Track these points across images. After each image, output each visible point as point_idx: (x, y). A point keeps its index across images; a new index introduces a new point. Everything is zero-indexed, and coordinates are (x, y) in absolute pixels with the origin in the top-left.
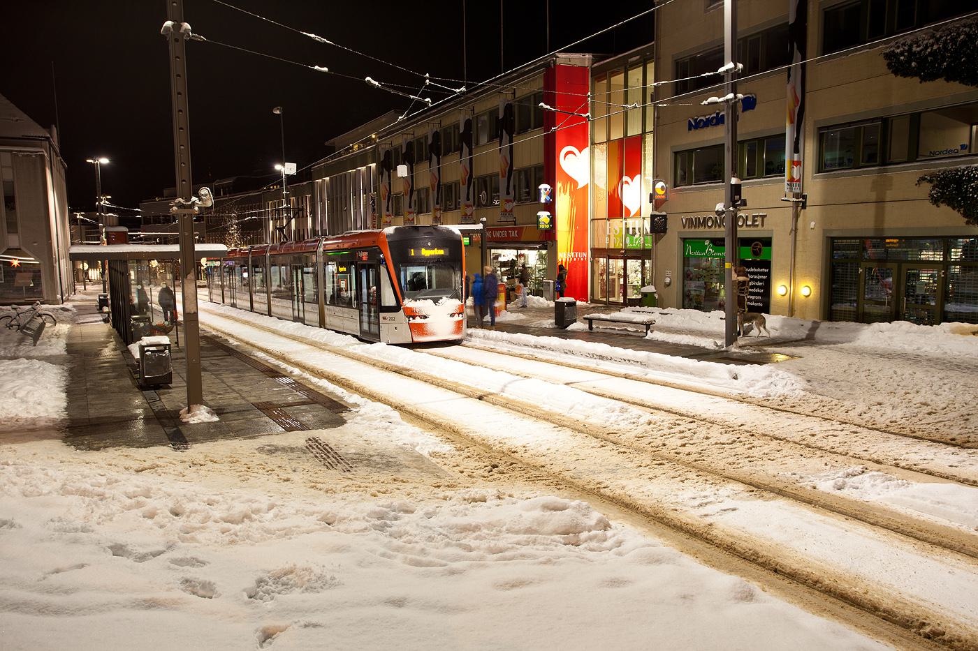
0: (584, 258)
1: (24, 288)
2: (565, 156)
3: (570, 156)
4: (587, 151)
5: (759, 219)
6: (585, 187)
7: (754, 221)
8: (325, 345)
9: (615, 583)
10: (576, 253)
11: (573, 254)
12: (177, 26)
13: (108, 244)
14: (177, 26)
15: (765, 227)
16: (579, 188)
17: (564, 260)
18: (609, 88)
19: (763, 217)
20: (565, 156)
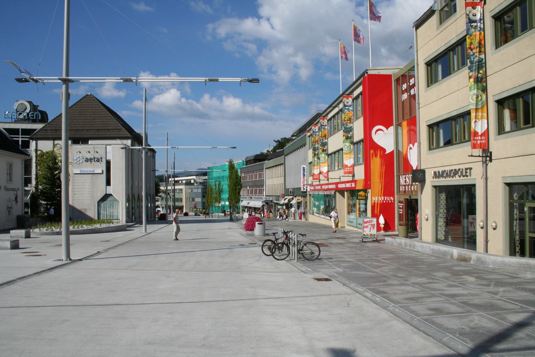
0: (391, 201)
1: (25, 176)
2: (376, 133)
3: (379, 132)
4: (392, 129)
5: (468, 171)
6: (392, 152)
7: (466, 172)
8: (515, 309)
9: (306, 313)
10: (386, 197)
11: (383, 198)
12: (55, 202)
13: (436, 172)
14: (55, 202)
15: (473, 177)
16: (386, 153)
17: (376, 202)
18: (104, 204)
19: (471, 169)
20: (376, 133)
